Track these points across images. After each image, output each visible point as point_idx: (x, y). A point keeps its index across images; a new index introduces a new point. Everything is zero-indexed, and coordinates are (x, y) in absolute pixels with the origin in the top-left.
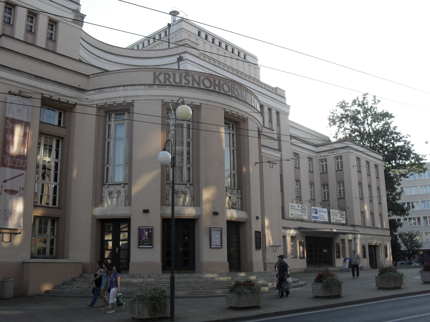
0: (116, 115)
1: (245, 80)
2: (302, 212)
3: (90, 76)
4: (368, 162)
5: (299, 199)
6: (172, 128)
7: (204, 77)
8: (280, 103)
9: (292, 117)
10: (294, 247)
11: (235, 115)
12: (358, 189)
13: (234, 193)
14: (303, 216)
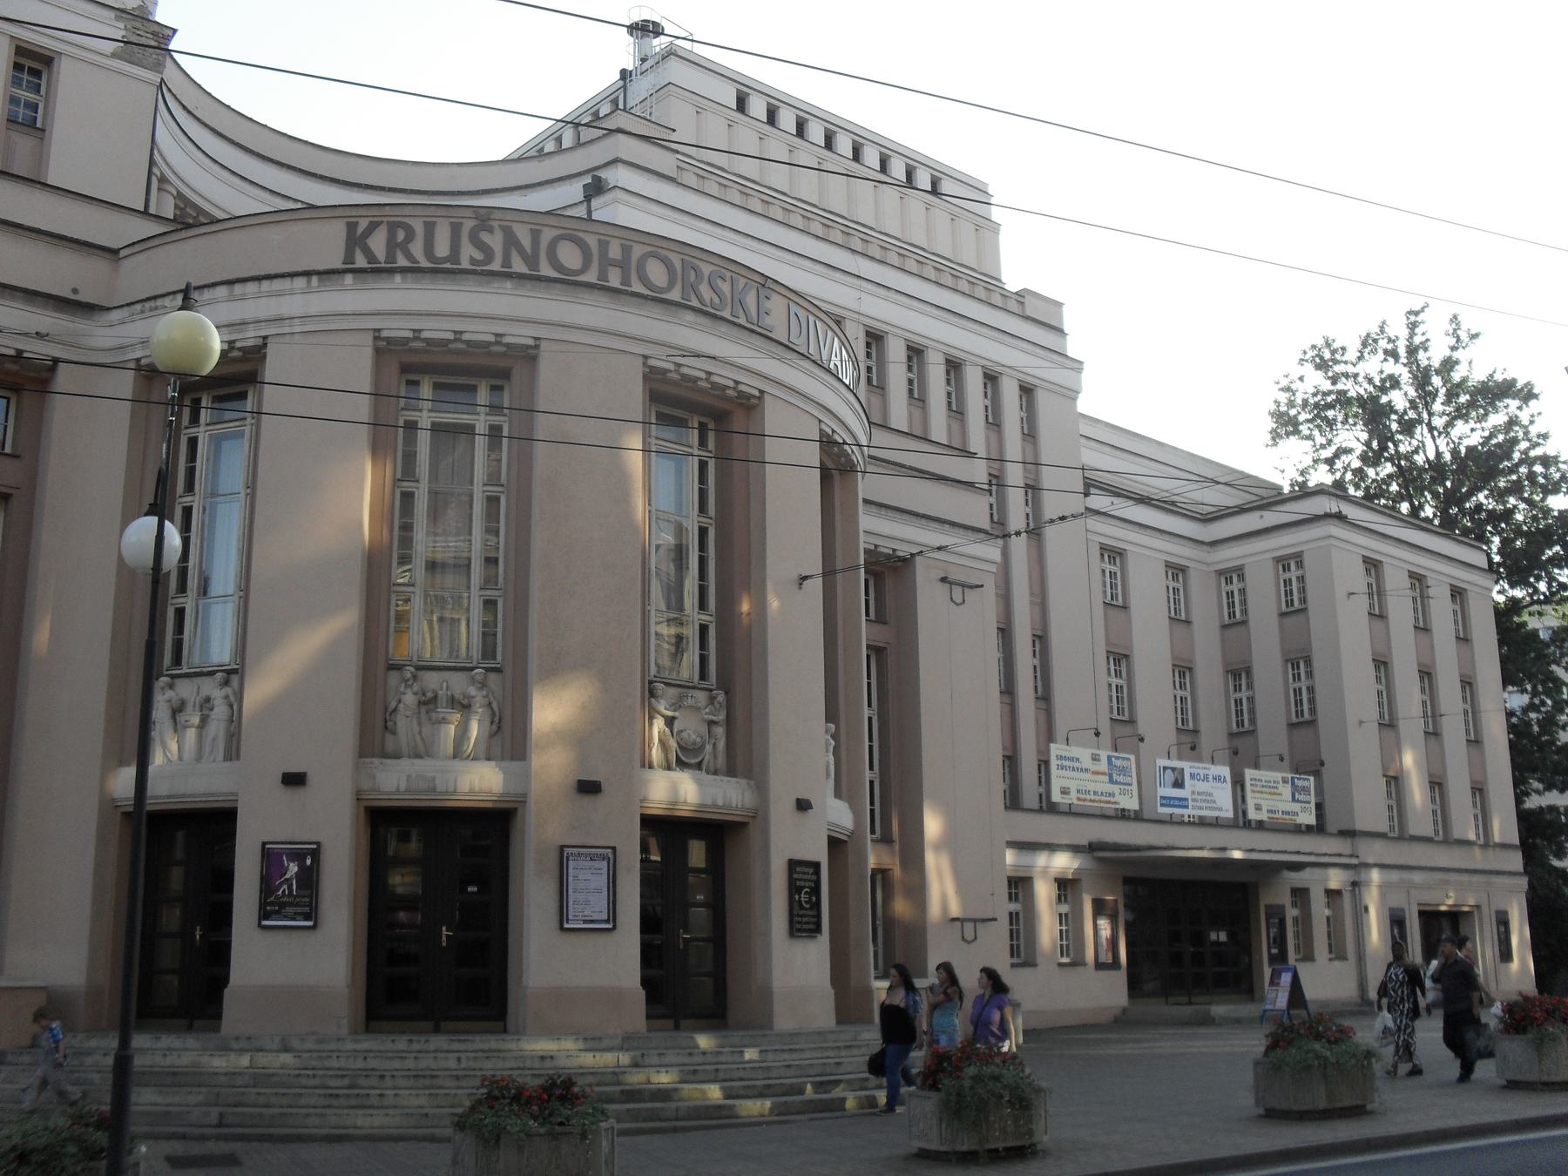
0: (219, 399)
2: (1111, 781)
3: (123, 253)
4: (1417, 579)
6: (424, 440)
7: (556, 233)
8: (1038, 350)
9: (1084, 405)
10: (1070, 924)
11: (702, 384)
12: (1373, 687)
13: (690, 702)
14: (1118, 798)
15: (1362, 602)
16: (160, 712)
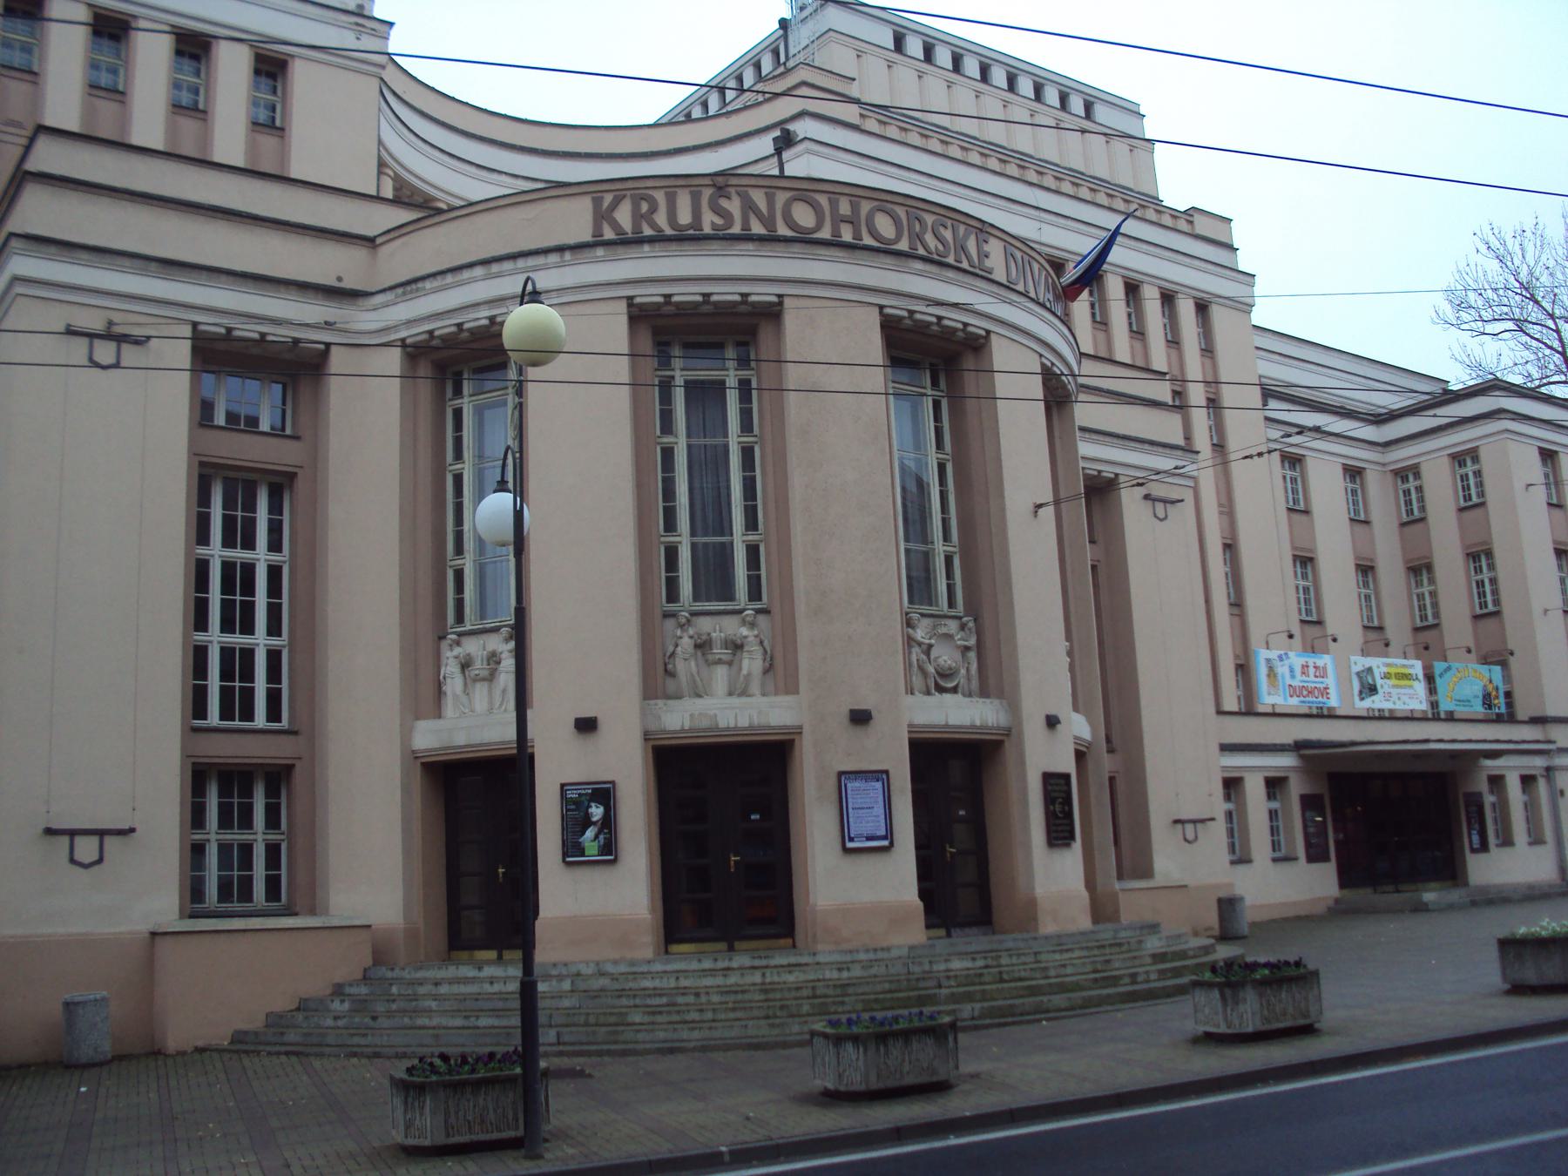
1: (1057, 192)
3: (379, 241)
5: (1312, 626)
9: (1258, 317)
13: (943, 630)
15: (1540, 494)
16: (451, 668)
